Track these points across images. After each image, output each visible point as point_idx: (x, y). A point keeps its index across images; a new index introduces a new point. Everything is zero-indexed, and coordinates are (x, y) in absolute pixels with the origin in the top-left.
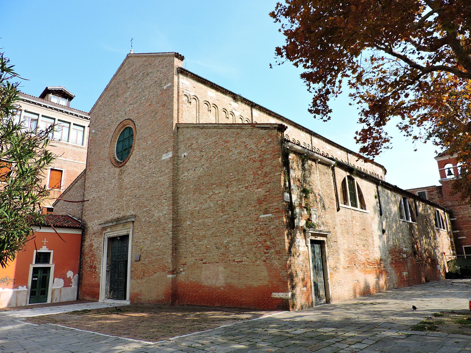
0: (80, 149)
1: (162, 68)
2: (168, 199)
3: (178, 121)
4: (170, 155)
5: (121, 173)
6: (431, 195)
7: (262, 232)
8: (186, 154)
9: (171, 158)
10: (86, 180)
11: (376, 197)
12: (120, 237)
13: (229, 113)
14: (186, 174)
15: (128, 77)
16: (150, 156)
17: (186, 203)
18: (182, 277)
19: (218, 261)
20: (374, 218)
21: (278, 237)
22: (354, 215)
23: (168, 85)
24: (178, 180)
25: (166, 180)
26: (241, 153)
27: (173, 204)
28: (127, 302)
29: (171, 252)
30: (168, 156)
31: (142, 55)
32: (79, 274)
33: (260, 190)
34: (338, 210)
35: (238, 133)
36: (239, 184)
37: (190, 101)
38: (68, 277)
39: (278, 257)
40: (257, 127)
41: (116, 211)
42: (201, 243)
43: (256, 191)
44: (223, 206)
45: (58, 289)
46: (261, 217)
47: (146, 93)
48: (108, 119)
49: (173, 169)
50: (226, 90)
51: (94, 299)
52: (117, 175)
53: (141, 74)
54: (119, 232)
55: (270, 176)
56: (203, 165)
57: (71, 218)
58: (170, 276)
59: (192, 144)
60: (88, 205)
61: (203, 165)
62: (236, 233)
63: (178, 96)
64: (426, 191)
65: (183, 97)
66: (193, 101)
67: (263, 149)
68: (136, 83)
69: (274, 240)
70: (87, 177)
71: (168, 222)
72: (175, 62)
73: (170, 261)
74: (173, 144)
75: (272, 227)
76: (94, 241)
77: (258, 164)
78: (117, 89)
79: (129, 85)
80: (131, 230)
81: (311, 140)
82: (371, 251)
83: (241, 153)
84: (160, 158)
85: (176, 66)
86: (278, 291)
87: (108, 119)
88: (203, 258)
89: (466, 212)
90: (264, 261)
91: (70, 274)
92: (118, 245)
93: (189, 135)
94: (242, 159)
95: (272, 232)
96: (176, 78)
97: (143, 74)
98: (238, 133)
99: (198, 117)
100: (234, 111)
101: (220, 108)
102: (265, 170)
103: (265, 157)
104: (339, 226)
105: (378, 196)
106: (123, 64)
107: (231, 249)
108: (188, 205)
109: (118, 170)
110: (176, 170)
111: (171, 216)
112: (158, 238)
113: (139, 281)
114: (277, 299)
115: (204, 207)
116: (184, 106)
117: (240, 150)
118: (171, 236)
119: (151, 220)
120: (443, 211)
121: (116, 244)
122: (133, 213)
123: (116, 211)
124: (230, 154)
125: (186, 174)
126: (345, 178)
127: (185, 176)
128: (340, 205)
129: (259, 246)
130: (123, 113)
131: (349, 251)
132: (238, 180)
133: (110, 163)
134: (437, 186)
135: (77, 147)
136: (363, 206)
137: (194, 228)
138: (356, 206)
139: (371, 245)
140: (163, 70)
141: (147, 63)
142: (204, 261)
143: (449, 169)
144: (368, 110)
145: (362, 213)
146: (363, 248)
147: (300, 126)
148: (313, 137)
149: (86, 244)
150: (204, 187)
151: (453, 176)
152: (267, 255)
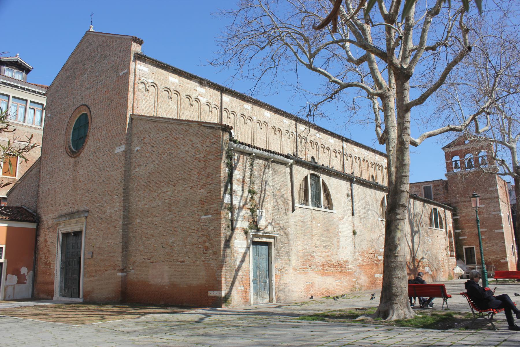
0: (37, 131)
1: (120, 52)
2: (119, 195)
3: (133, 112)
4: (123, 148)
5: (76, 164)
6: (436, 190)
7: (203, 233)
8: (138, 148)
9: (123, 151)
10: (41, 169)
11: (348, 195)
12: (74, 233)
13: (194, 100)
14: (138, 170)
15: (85, 57)
16: (104, 147)
17: (137, 200)
18: (134, 274)
19: (164, 260)
20: (343, 218)
21: (216, 238)
22: (314, 215)
23: (124, 72)
24: (130, 175)
25: (117, 174)
26: (188, 151)
27: (124, 201)
28: (80, 300)
29: (121, 250)
30: (120, 149)
31: (101, 34)
32: (34, 271)
33: (202, 190)
34: (293, 210)
35: (187, 131)
36: (185, 183)
37: (147, 88)
38: (22, 273)
39: (214, 258)
41: (70, 205)
42: (149, 242)
43: (199, 191)
44: (169, 205)
45: (11, 285)
46: (202, 217)
47: (103, 77)
48: (64, 102)
49: (125, 164)
50: (190, 75)
51: (50, 297)
52: (71, 165)
53: (99, 55)
54: (72, 227)
55: (212, 177)
56: (154, 161)
57: (26, 210)
58: (120, 274)
59: (145, 138)
60: (42, 197)
61: (154, 161)
62: (180, 233)
63: (134, 84)
64: (432, 185)
65: (139, 85)
66: (152, 89)
67: (208, 149)
68: (93, 65)
69: (212, 241)
70: (42, 166)
71: (119, 219)
72: (133, 46)
73: (120, 259)
74: (125, 137)
75: (211, 228)
76: (48, 237)
77: (202, 164)
78: (75, 69)
79: (86, 67)
80: (84, 226)
81: (296, 127)
82: (334, 253)
83: (188, 151)
84: (114, 151)
85: (134, 51)
86: (213, 290)
87: (64, 102)
88: (150, 257)
90: (203, 261)
91: (24, 270)
92: (71, 239)
93: (142, 128)
94: (189, 158)
95: (211, 233)
96: (132, 64)
97: (101, 56)
98: (187, 131)
99: (156, 107)
100: (199, 98)
101: (183, 95)
102: (208, 170)
103: (209, 157)
104: (293, 227)
105: (351, 195)
106: (81, 42)
107: (175, 249)
108: (139, 202)
109: (72, 160)
110: (128, 165)
111: (122, 213)
112: (110, 235)
113: (91, 279)
114: (212, 297)
115: (153, 205)
116: (140, 94)
117: (187, 149)
118: (121, 233)
119: (103, 216)
120: (443, 209)
121: (71, 240)
122: (86, 208)
123: (70, 205)
124: (179, 152)
125: (138, 170)
126: (307, 177)
127: (139, 171)
128: (297, 205)
130: (79, 98)
131: (304, 252)
132: (184, 179)
133: (65, 152)
135: (35, 128)
136: (330, 205)
137: (143, 226)
138: (318, 205)
139: (336, 246)
140: (121, 54)
141: (105, 44)
142: (152, 260)
145: (326, 213)
146: (324, 250)
147: (282, 111)
148: (298, 124)
149: (41, 239)
150: (153, 184)
152: (205, 255)
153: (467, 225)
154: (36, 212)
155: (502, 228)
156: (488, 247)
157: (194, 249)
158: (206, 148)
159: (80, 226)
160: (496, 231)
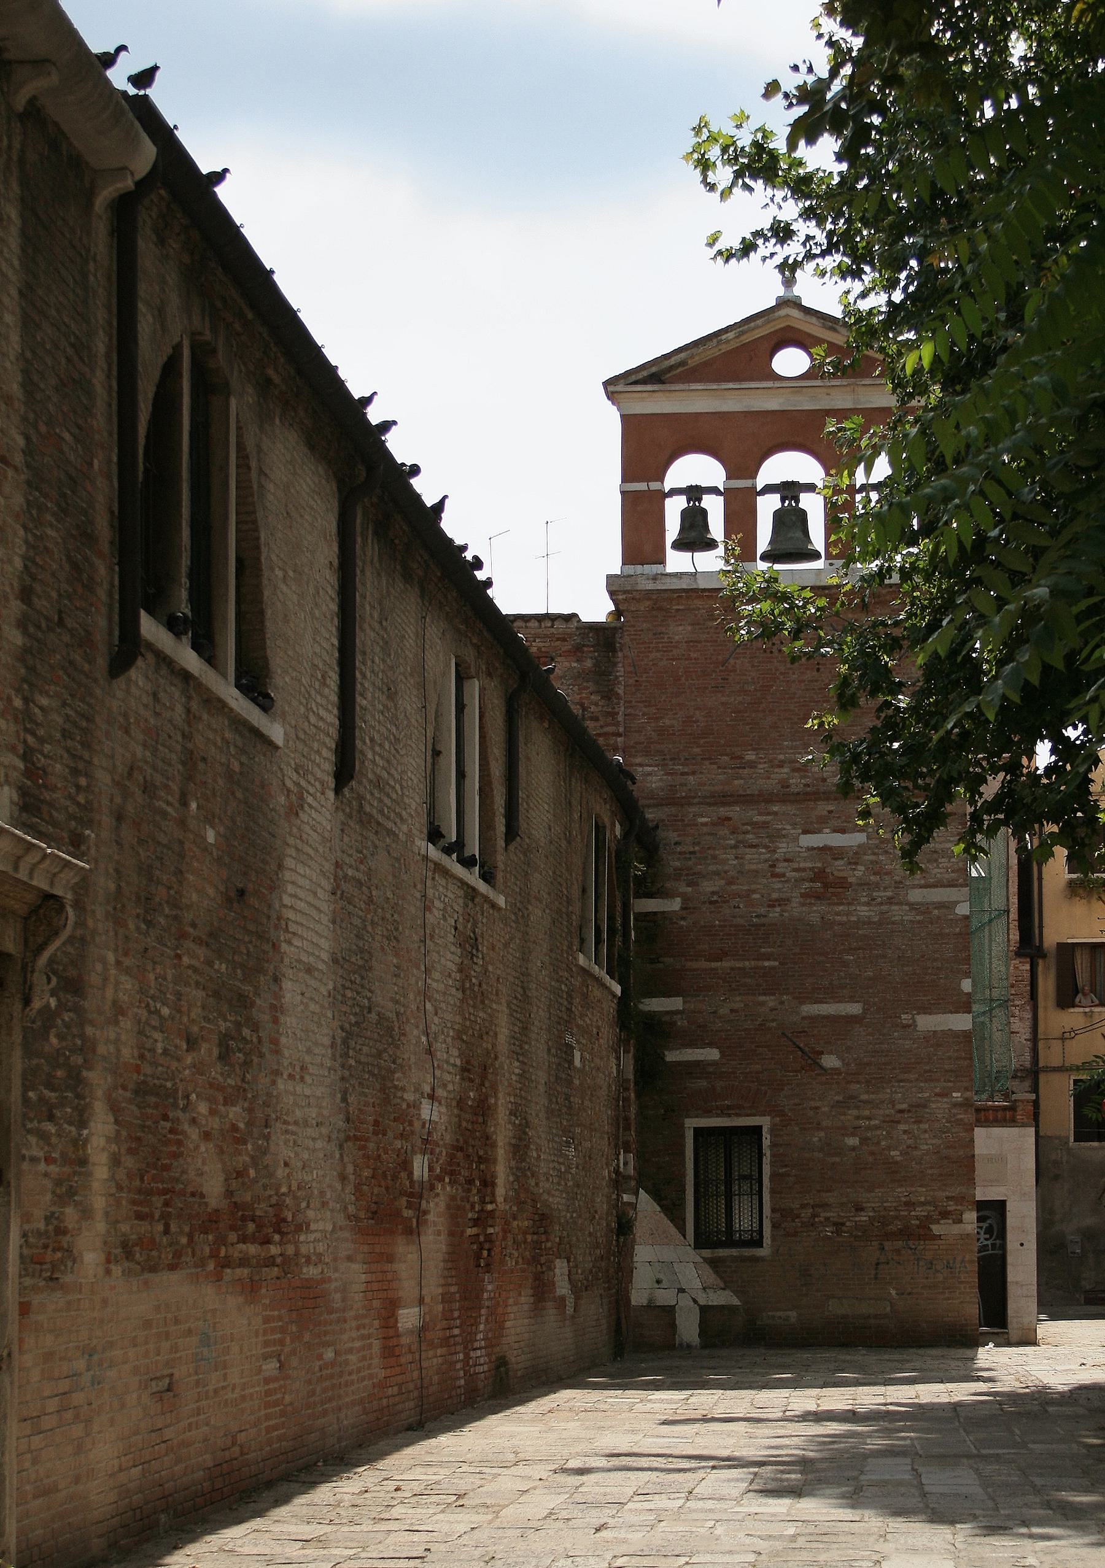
89: (754, 859)
134: (585, 618)
143: (694, 493)
144: (844, 167)
151: (710, 562)
153: (726, 964)
155: (622, 493)
156: (855, 1130)
160: (927, 1022)
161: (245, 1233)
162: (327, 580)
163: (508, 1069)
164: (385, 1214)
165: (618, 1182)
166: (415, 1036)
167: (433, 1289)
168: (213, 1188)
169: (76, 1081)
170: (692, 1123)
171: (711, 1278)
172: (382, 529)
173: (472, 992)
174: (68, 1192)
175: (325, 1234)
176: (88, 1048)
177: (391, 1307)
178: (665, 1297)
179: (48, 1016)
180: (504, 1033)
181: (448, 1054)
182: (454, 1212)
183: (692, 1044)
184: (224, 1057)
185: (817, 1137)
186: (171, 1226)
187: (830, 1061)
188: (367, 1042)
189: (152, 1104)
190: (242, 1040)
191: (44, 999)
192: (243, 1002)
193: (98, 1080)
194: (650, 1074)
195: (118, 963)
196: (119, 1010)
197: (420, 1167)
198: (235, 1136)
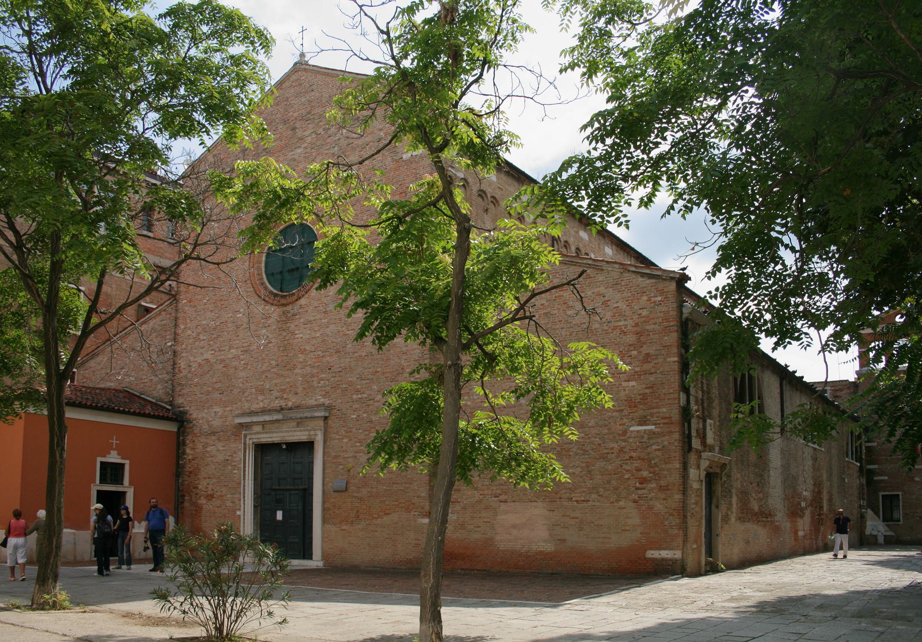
5: (286, 318)
12: (288, 444)
21: (666, 463)
28: (316, 562)
40: (633, 272)
43: (624, 384)
46: (632, 429)
62: (576, 454)
79: (299, 133)
109: (274, 312)
129: (626, 477)
142: (502, 497)
152: (640, 492)
154: (171, 403)
157: (613, 482)
158: (641, 311)
159: (307, 433)
161: (764, 516)
162: (778, 396)
163: (826, 484)
164: (795, 513)
165: (860, 507)
166: (801, 479)
167: (807, 528)
168: (756, 508)
169: (730, 491)
170: (881, 494)
171: (886, 528)
172: (790, 383)
173: (816, 469)
174: (729, 509)
175: (780, 517)
176: (732, 486)
177: (796, 532)
178: (875, 533)
179: (725, 482)
180: (825, 476)
181: (810, 482)
182: (812, 513)
183: (881, 475)
184: (758, 485)
185: (914, 497)
186: (747, 514)
187: (917, 479)
188: (790, 482)
189: (744, 496)
190: (762, 481)
191: (724, 479)
192: (762, 476)
193: (734, 491)
194: (870, 482)
195: (233, 20)
196: (737, 479)
197: (803, 504)
198: (761, 499)
